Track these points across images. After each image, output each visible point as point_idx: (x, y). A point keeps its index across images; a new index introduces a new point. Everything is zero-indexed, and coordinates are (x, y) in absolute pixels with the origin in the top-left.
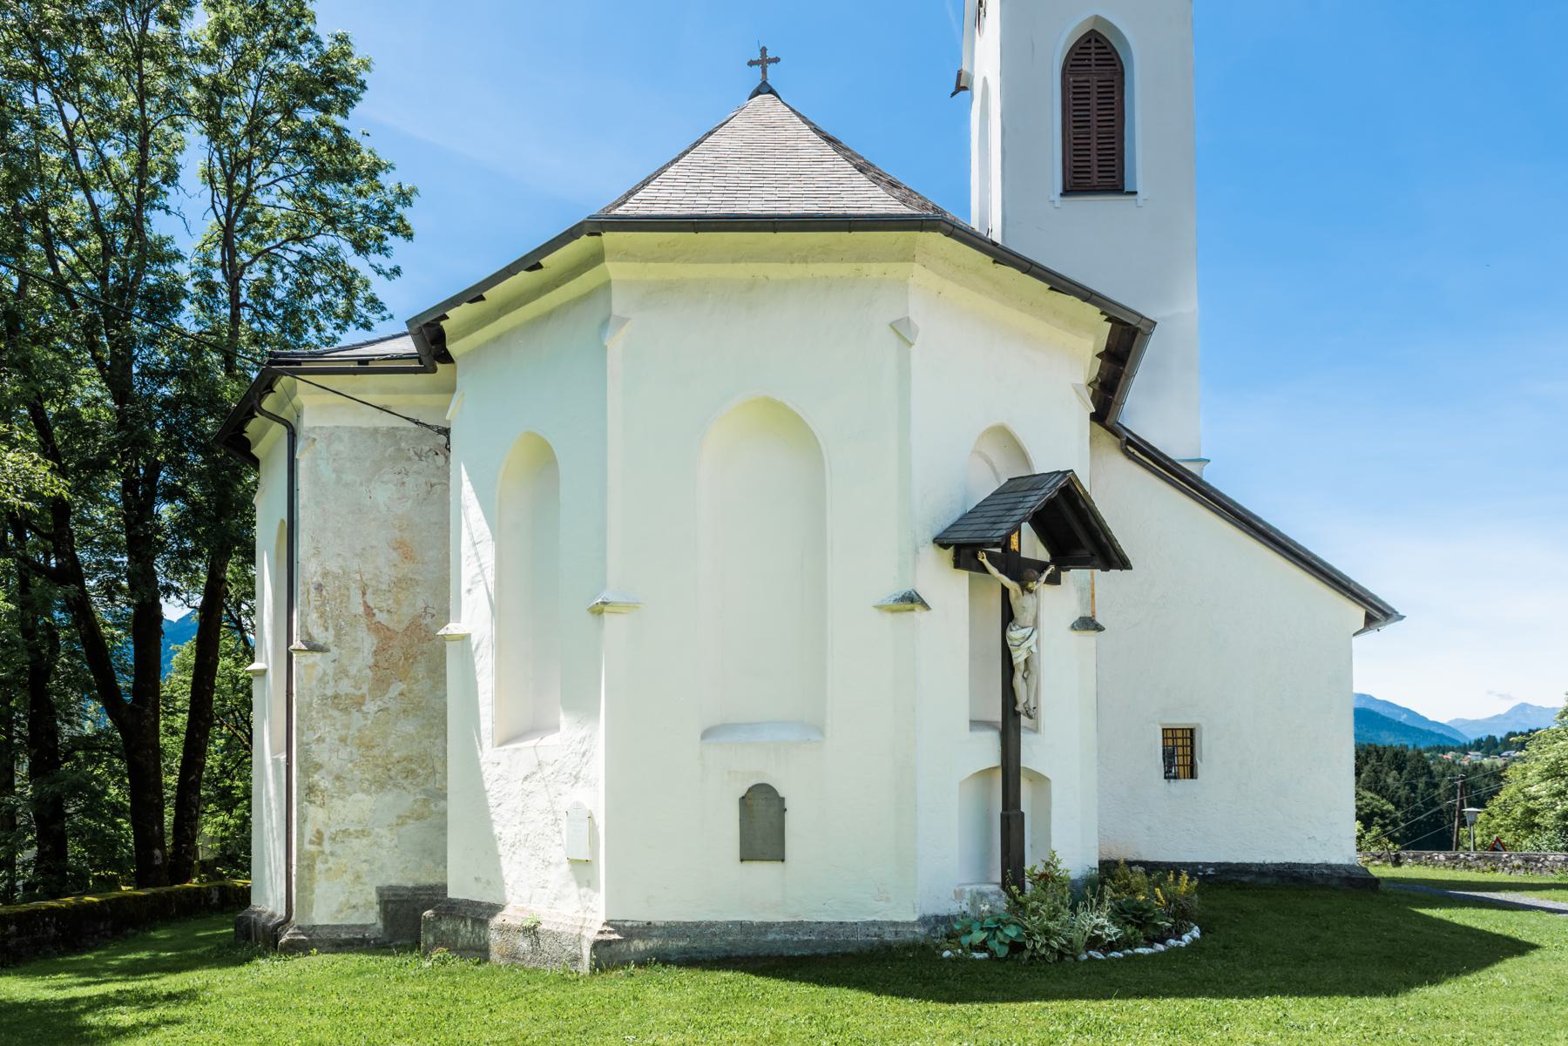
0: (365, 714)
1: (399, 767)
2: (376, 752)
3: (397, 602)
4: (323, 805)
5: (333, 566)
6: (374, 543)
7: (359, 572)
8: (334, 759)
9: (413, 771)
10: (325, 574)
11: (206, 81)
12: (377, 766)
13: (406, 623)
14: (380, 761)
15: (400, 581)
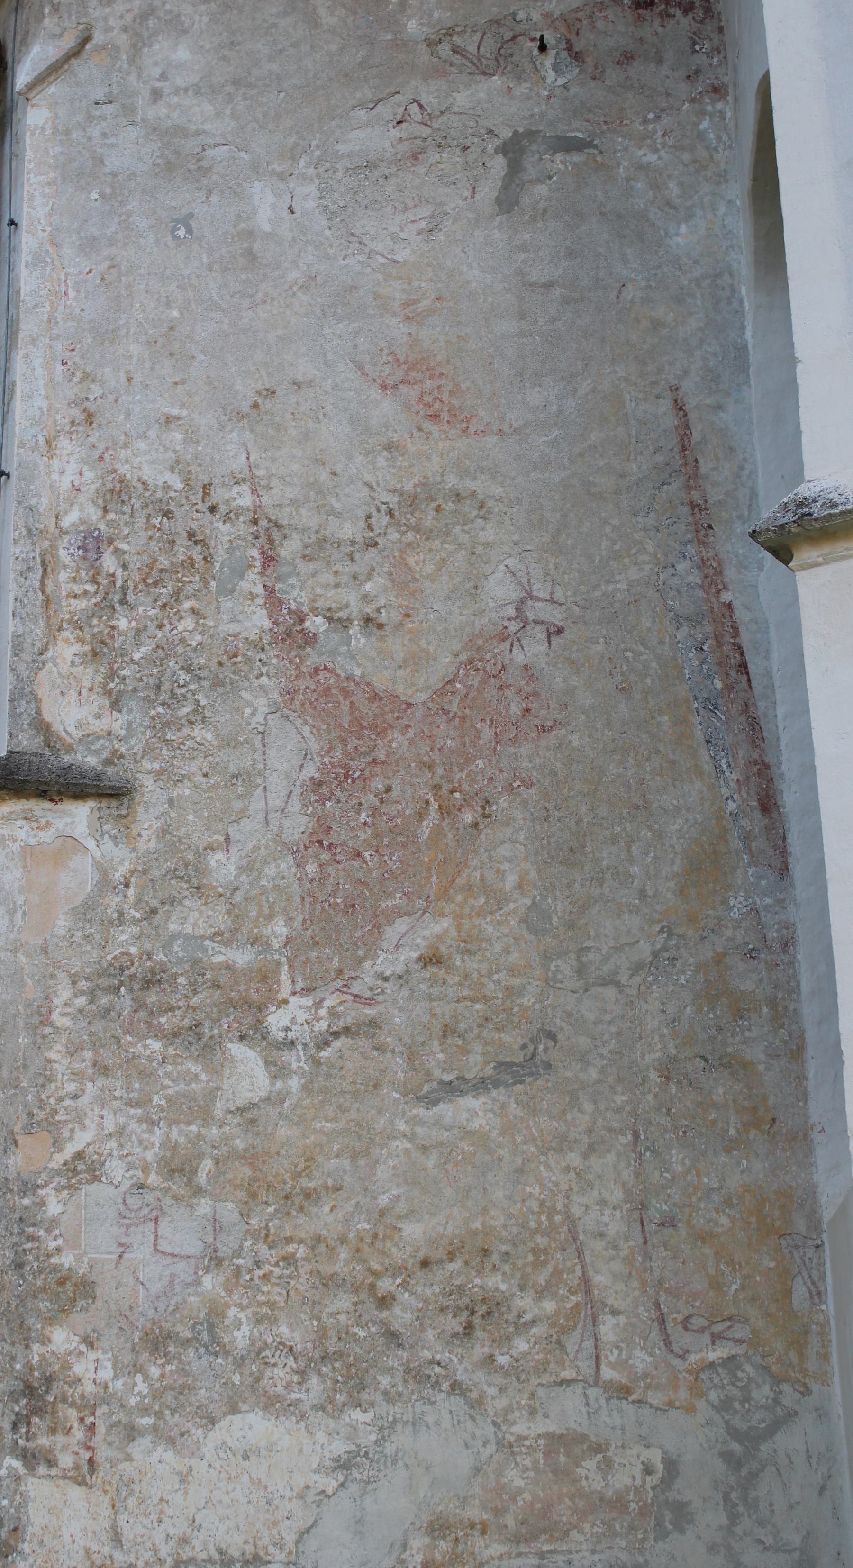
0: (275, 1048)
1: (429, 1288)
2: (325, 1218)
3: (404, 582)
4: (86, 1473)
5: (148, 464)
6: (305, 369)
7: (249, 479)
8: (141, 1252)
9: (493, 1306)
10: (116, 493)
11: (489, 1071)
12: (329, 1283)
13: (444, 664)
14: (341, 1263)
15: (412, 501)
